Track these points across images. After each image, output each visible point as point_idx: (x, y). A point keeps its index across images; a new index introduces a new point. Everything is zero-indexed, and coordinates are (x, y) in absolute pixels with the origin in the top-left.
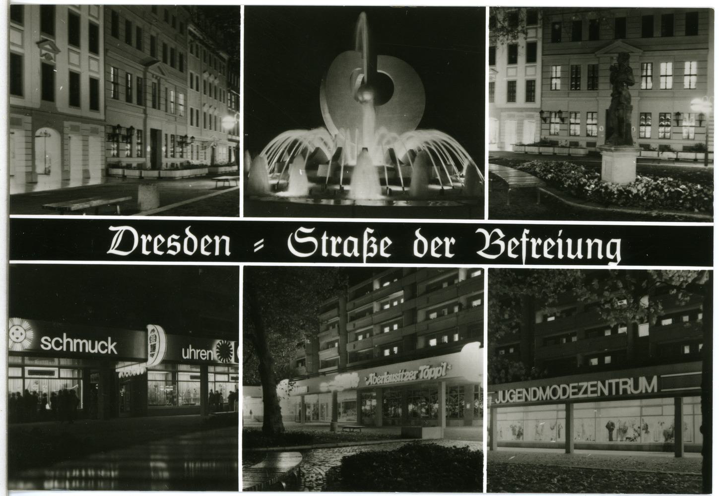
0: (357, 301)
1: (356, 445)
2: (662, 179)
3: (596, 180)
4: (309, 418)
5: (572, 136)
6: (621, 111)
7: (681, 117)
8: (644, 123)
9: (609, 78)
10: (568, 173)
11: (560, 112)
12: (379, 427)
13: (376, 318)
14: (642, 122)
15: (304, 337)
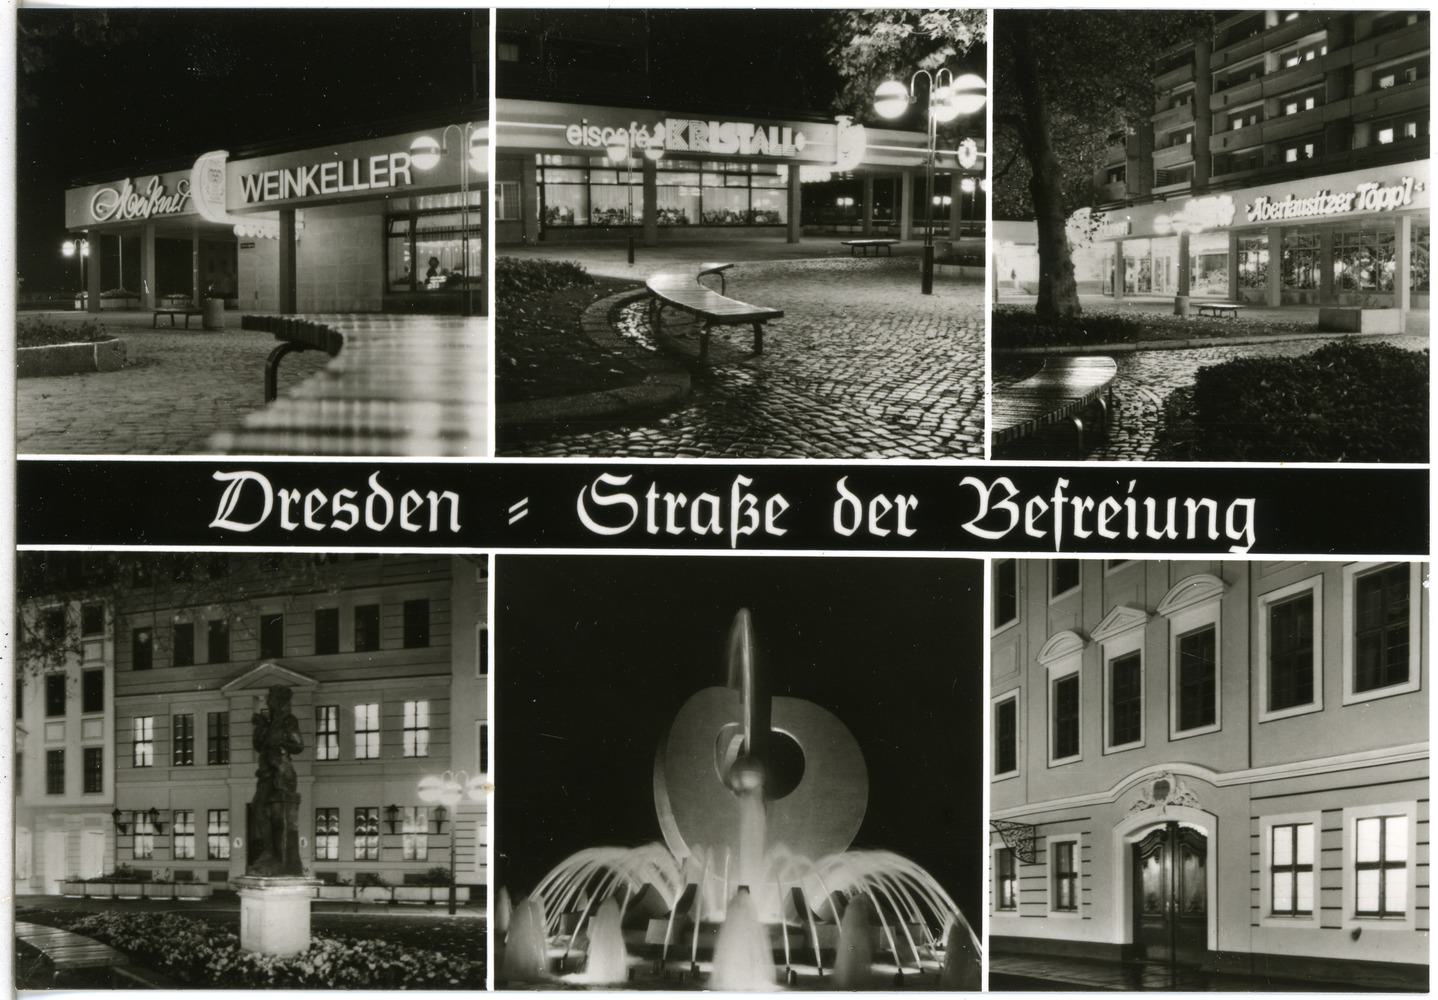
0: (1233, 51)
1: (1227, 345)
2: (364, 943)
3: (230, 949)
4: (1131, 288)
5: (180, 859)
6: (277, 806)
7: (399, 816)
8: (324, 829)
9: (251, 738)
10: (173, 936)
11: (154, 812)
12: (1274, 309)
13: (1271, 85)
14: (319, 828)
15: (1122, 122)
